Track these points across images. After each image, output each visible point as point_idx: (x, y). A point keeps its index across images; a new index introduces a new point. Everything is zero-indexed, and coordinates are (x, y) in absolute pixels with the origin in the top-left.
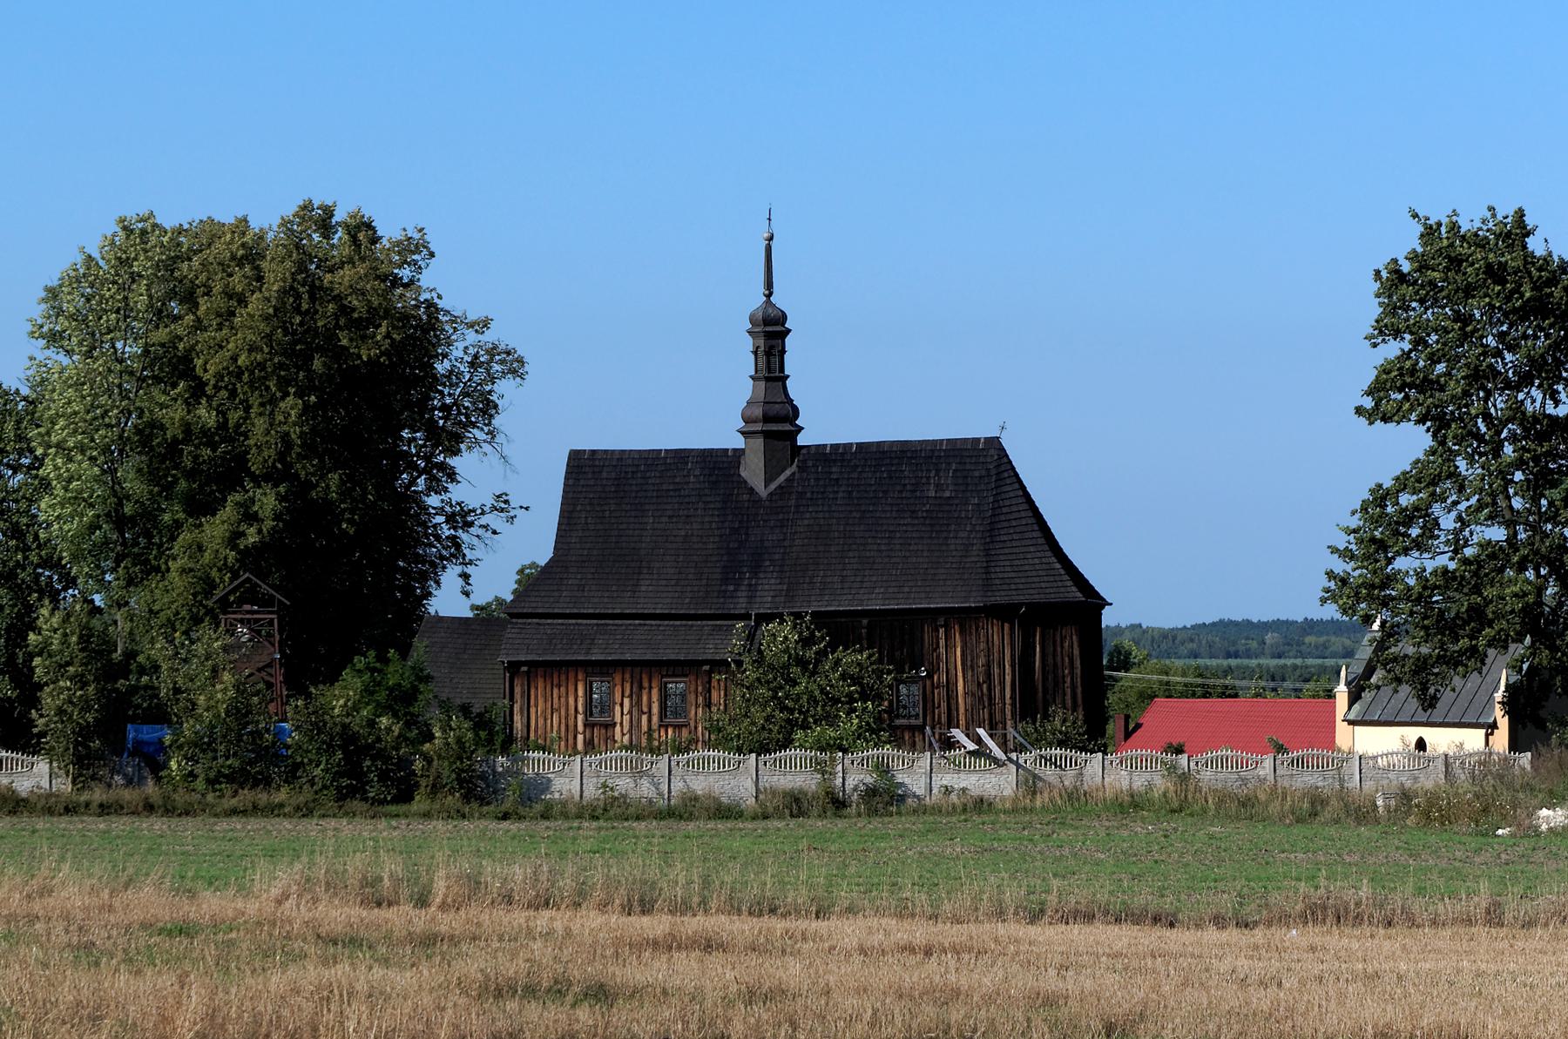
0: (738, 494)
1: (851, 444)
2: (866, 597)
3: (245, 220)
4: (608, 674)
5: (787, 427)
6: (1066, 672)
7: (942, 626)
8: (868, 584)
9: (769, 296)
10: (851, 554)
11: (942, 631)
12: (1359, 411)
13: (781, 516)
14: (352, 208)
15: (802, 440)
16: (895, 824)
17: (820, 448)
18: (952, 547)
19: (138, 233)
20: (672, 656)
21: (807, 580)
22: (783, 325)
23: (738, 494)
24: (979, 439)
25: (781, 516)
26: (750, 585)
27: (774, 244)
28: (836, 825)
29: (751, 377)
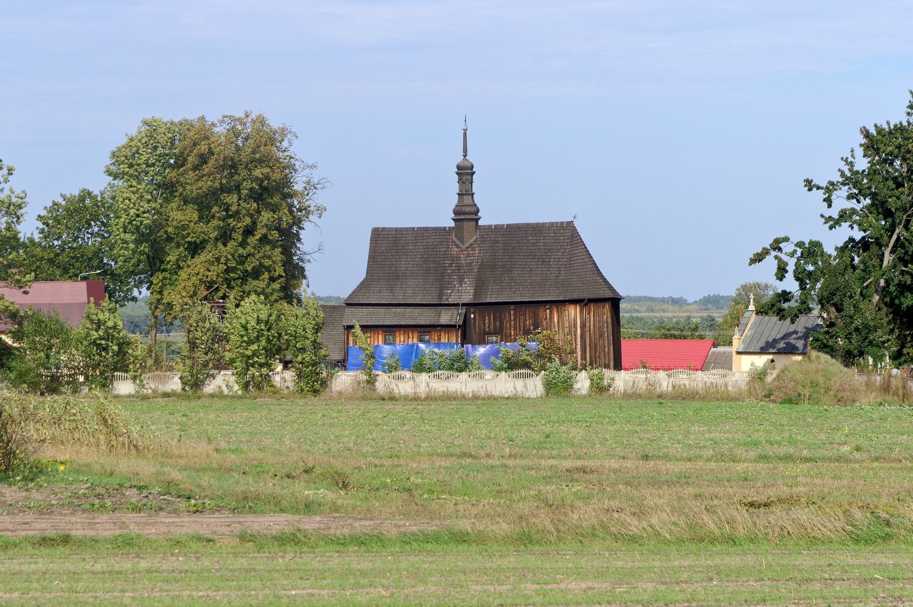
0: (451, 248)
1: (503, 225)
2: (513, 295)
3: (203, 118)
4: (393, 332)
5: (474, 217)
6: (605, 329)
7: (548, 309)
8: (514, 290)
9: (465, 156)
10: (505, 276)
11: (548, 311)
12: (831, 228)
13: (472, 258)
14: (258, 113)
15: (481, 223)
16: (264, 401)
17: (498, 228)
18: (552, 272)
19: (152, 127)
20: (423, 323)
21: (490, 290)
22: (472, 169)
23: (451, 248)
24: (563, 222)
25: (472, 258)
26: (458, 290)
27: (468, 132)
28: (17, 407)
29: (457, 194)
